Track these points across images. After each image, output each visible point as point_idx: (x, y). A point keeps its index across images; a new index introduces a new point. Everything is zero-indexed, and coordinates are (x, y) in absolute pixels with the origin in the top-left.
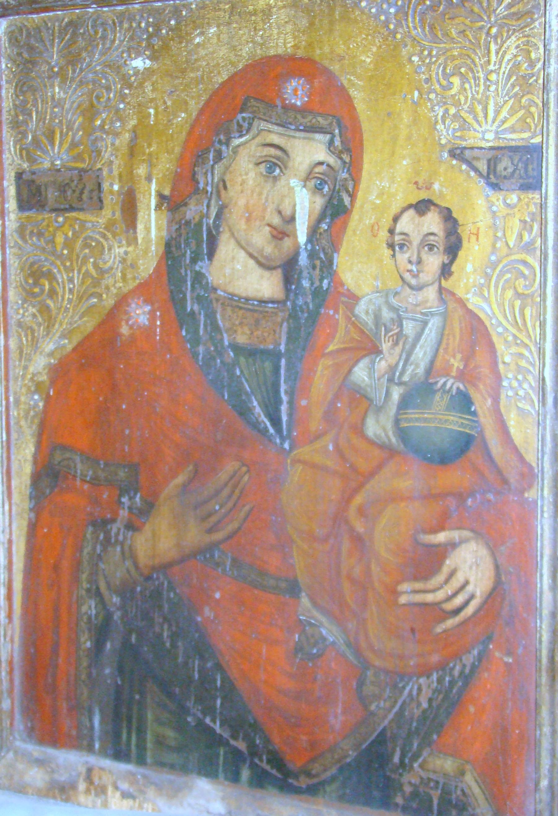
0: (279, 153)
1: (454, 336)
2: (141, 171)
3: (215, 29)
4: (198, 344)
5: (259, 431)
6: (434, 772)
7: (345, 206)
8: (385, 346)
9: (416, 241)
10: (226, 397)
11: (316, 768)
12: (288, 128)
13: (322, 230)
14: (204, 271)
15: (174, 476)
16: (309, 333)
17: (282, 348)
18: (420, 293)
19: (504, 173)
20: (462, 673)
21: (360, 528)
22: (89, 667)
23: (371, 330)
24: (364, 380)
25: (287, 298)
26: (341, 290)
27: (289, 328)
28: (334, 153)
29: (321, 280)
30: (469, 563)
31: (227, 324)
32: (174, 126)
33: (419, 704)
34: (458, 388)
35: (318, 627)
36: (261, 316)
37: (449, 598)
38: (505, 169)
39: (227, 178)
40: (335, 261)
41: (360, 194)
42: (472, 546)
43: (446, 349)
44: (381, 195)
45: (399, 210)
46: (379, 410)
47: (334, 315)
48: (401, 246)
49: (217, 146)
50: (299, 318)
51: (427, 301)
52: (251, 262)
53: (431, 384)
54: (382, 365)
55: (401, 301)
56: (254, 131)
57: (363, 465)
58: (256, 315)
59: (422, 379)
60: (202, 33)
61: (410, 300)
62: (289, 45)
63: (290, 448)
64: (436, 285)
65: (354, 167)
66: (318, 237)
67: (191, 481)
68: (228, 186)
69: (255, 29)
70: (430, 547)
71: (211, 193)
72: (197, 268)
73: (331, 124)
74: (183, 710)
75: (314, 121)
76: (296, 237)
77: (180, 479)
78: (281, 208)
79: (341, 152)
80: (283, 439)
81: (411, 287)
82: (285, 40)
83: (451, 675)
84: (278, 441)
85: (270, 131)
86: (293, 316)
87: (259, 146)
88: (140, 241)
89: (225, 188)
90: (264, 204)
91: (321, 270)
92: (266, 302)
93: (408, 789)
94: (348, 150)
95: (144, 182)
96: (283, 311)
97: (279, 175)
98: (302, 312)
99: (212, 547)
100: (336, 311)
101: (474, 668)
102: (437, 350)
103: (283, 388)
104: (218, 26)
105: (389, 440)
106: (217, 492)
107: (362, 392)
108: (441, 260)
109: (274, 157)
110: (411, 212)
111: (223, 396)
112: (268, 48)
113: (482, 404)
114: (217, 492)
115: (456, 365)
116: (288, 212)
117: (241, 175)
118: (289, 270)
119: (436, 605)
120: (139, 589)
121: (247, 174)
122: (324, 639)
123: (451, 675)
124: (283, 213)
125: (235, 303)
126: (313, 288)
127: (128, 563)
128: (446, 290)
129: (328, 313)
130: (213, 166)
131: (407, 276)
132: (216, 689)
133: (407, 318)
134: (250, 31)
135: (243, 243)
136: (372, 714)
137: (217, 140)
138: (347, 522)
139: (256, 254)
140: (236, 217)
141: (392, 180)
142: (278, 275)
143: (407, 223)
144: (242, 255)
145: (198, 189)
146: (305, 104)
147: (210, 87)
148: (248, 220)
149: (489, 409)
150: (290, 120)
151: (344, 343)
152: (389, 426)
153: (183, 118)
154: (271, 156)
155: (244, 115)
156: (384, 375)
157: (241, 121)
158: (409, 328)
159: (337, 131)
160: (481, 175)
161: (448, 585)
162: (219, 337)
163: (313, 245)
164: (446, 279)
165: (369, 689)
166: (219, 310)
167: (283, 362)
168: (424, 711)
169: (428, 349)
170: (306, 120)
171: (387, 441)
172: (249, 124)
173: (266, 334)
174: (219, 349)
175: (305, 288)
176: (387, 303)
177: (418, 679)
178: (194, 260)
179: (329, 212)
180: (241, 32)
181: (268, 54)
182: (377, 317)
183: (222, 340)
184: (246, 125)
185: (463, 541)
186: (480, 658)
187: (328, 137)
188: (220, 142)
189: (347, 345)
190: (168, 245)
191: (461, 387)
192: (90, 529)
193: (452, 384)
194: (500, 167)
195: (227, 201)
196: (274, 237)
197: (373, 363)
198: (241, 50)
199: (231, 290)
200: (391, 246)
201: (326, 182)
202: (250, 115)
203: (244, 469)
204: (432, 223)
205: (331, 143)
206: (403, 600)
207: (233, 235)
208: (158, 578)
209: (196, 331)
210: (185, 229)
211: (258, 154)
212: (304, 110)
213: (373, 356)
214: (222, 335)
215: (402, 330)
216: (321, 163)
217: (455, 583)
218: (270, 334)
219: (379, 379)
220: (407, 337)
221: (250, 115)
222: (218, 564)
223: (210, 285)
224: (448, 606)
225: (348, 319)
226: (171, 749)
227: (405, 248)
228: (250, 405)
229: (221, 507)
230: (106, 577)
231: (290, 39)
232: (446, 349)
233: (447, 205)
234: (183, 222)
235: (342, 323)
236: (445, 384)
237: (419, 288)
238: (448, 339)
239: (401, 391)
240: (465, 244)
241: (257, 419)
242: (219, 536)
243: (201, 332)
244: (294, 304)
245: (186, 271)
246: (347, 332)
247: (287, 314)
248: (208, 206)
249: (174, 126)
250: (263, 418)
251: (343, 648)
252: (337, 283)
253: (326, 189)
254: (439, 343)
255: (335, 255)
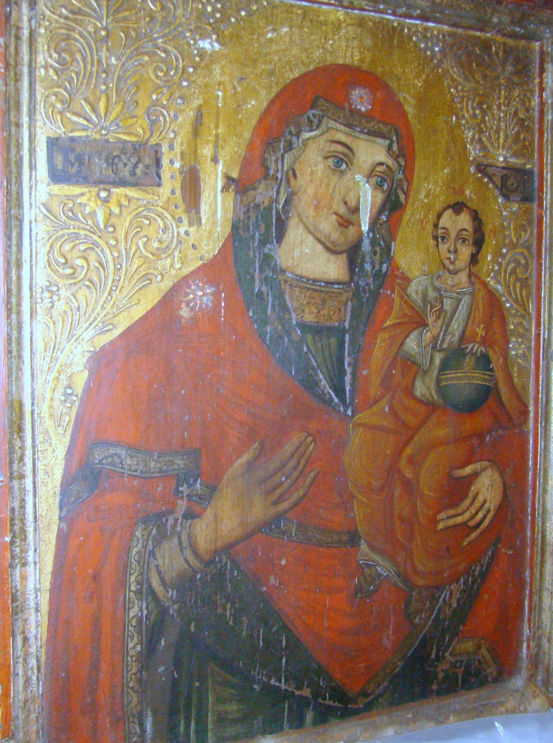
0: (345, 150)
1: (479, 311)
2: (207, 151)
3: (288, 29)
4: (266, 324)
5: (325, 402)
6: (460, 654)
7: (401, 203)
8: (430, 320)
9: (453, 236)
10: (293, 373)
11: (371, 687)
12: (354, 129)
13: (382, 221)
14: (272, 253)
15: (238, 458)
16: (371, 311)
17: (347, 325)
18: (456, 276)
19: (511, 188)
20: (481, 571)
21: (408, 473)
22: (140, 671)
23: (420, 307)
24: (414, 349)
25: (351, 279)
26: (397, 273)
27: (353, 307)
28: (392, 156)
29: (381, 264)
30: (487, 485)
31: (296, 305)
32: (244, 111)
33: (451, 605)
34: (481, 351)
35: (376, 566)
36: (327, 296)
37: (473, 517)
38: (512, 184)
39: (297, 167)
40: (393, 248)
41: (412, 193)
42: (489, 472)
43: (473, 321)
44: (427, 195)
45: (441, 209)
46: (425, 372)
47: (391, 294)
48: (443, 238)
49: (288, 137)
50: (362, 298)
51: (460, 283)
52: (319, 247)
53: (463, 349)
54: (428, 336)
55: (442, 283)
56: (323, 127)
57: (411, 420)
58: (322, 295)
59: (457, 346)
60: (274, 30)
61: (449, 283)
62: (356, 58)
63: (352, 414)
64: (467, 270)
65: (408, 170)
66: (378, 226)
67: (256, 458)
68: (298, 175)
69: (325, 38)
70: (459, 479)
71: (281, 180)
72: (266, 251)
73: (389, 132)
74: (248, 679)
75: (376, 127)
76: (360, 226)
77: (245, 458)
78: (347, 199)
79: (398, 156)
80: (346, 407)
81: (450, 272)
82: (352, 53)
83: (473, 576)
84: (342, 409)
85: (337, 130)
86: (356, 294)
87: (327, 141)
88: (204, 221)
89: (295, 176)
90: (331, 195)
91: (381, 255)
92: (332, 283)
93: (441, 675)
94: (404, 156)
95: (209, 164)
96: (348, 292)
97: (345, 170)
98: (365, 292)
99: (278, 517)
100: (393, 292)
101: (489, 564)
102: (467, 323)
103: (347, 361)
104: (291, 27)
105: (432, 397)
106: (283, 466)
107: (412, 359)
108: (470, 250)
109: (339, 153)
110: (449, 212)
111: (291, 373)
112: (337, 57)
113: (496, 363)
114: (283, 466)
115: (480, 333)
116: (352, 203)
117: (310, 166)
118: (353, 254)
119: (464, 523)
120: (199, 576)
121: (316, 166)
122: (380, 575)
123: (473, 576)
124: (349, 204)
125: (302, 285)
126: (374, 272)
127: (188, 553)
128: (474, 274)
129: (386, 293)
130: (283, 155)
131: (447, 262)
132: (282, 650)
133: (446, 297)
134: (321, 38)
135: (311, 228)
136: (416, 625)
137: (287, 131)
138: (399, 472)
139: (323, 240)
140: (304, 204)
141: (436, 183)
142: (343, 260)
143: (447, 220)
144: (311, 239)
145: (269, 175)
146: (367, 111)
147: (281, 80)
148: (317, 208)
149: (501, 366)
150: (356, 123)
151: (398, 318)
152: (432, 386)
153: (253, 106)
154: (339, 153)
155: (314, 112)
156: (429, 344)
157: (311, 117)
158: (448, 304)
159: (394, 138)
160: (497, 187)
161: (473, 506)
162: (287, 316)
163: (374, 234)
164: (473, 266)
165: (414, 605)
166: (288, 290)
167: (347, 336)
168: (454, 610)
169: (461, 322)
170: (369, 125)
171: (431, 399)
172: (318, 120)
173: (332, 313)
174: (287, 328)
175: (367, 272)
176: (432, 284)
177: (450, 586)
178: (264, 242)
179: (388, 206)
180: (312, 37)
181: (337, 62)
182: (425, 296)
183: (290, 319)
184: (316, 121)
185: (483, 470)
186: (492, 557)
187: (388, 142)
188: (290, 133)
189: (400, 320)
190: (235, 227)
191: (483, 349)
192: (141, 527)
193: (478, 348)
194: (509, 182)
195: (297, 189)
196: (340, 224)
197: (421, 335)
198: (312, 53)
199: (299, 272)
200: (435, 238)
201: (385, 180)
202: (321, 114)
203: (310, 439)
204: (464, 221)
205: (390, 148)
206: (440, 526)
207: (301, 220)
208: (220, 561)
209: (264, 312)
210: (254, 212)
211: (327, 149)
212: (368, 116)
213: (421, 329)
214: (290, 314)
215: (442, 307)
216: (381, 164)
217: (477, 504)
218: (335, 312)
219: (425, 347)
220: (446, 311)
221: (321, 114)
222: (283, 533)
223: (278, 267)
224: (472, 523)
225: (402, 297)
226: (235, 721)
227: (446, 240)
228: (317, 379)
229: (286, 479)
230: (159, 573)
231: (356, 52)
232: (473, 321)
233: (475, 208)
234: (252, 205)
235: (397, 301)
236: (472, 349)
237: (455, 273)
238: (475, 313)
239: (442, 356)
240: (487, 237)
241: (323, 391)
242: (285, 505)
243: (269, 313)
244: (357, 286)
245: (254, 253)
246: (401, 309)
247: (351, 294)
248: (278, 192)
249: (244, 111)
250: (328, 390)
251: (395, 578)
252: (394, 267)
253: (385, 186)
254: (469, 316)
255: (393, 243)
